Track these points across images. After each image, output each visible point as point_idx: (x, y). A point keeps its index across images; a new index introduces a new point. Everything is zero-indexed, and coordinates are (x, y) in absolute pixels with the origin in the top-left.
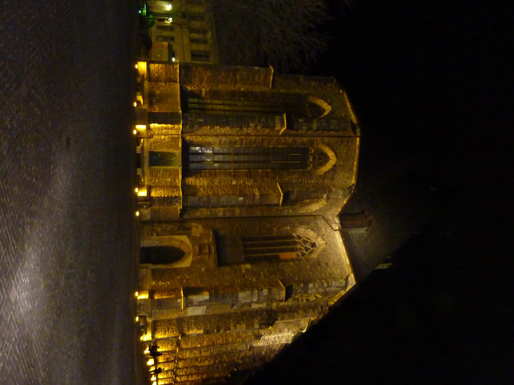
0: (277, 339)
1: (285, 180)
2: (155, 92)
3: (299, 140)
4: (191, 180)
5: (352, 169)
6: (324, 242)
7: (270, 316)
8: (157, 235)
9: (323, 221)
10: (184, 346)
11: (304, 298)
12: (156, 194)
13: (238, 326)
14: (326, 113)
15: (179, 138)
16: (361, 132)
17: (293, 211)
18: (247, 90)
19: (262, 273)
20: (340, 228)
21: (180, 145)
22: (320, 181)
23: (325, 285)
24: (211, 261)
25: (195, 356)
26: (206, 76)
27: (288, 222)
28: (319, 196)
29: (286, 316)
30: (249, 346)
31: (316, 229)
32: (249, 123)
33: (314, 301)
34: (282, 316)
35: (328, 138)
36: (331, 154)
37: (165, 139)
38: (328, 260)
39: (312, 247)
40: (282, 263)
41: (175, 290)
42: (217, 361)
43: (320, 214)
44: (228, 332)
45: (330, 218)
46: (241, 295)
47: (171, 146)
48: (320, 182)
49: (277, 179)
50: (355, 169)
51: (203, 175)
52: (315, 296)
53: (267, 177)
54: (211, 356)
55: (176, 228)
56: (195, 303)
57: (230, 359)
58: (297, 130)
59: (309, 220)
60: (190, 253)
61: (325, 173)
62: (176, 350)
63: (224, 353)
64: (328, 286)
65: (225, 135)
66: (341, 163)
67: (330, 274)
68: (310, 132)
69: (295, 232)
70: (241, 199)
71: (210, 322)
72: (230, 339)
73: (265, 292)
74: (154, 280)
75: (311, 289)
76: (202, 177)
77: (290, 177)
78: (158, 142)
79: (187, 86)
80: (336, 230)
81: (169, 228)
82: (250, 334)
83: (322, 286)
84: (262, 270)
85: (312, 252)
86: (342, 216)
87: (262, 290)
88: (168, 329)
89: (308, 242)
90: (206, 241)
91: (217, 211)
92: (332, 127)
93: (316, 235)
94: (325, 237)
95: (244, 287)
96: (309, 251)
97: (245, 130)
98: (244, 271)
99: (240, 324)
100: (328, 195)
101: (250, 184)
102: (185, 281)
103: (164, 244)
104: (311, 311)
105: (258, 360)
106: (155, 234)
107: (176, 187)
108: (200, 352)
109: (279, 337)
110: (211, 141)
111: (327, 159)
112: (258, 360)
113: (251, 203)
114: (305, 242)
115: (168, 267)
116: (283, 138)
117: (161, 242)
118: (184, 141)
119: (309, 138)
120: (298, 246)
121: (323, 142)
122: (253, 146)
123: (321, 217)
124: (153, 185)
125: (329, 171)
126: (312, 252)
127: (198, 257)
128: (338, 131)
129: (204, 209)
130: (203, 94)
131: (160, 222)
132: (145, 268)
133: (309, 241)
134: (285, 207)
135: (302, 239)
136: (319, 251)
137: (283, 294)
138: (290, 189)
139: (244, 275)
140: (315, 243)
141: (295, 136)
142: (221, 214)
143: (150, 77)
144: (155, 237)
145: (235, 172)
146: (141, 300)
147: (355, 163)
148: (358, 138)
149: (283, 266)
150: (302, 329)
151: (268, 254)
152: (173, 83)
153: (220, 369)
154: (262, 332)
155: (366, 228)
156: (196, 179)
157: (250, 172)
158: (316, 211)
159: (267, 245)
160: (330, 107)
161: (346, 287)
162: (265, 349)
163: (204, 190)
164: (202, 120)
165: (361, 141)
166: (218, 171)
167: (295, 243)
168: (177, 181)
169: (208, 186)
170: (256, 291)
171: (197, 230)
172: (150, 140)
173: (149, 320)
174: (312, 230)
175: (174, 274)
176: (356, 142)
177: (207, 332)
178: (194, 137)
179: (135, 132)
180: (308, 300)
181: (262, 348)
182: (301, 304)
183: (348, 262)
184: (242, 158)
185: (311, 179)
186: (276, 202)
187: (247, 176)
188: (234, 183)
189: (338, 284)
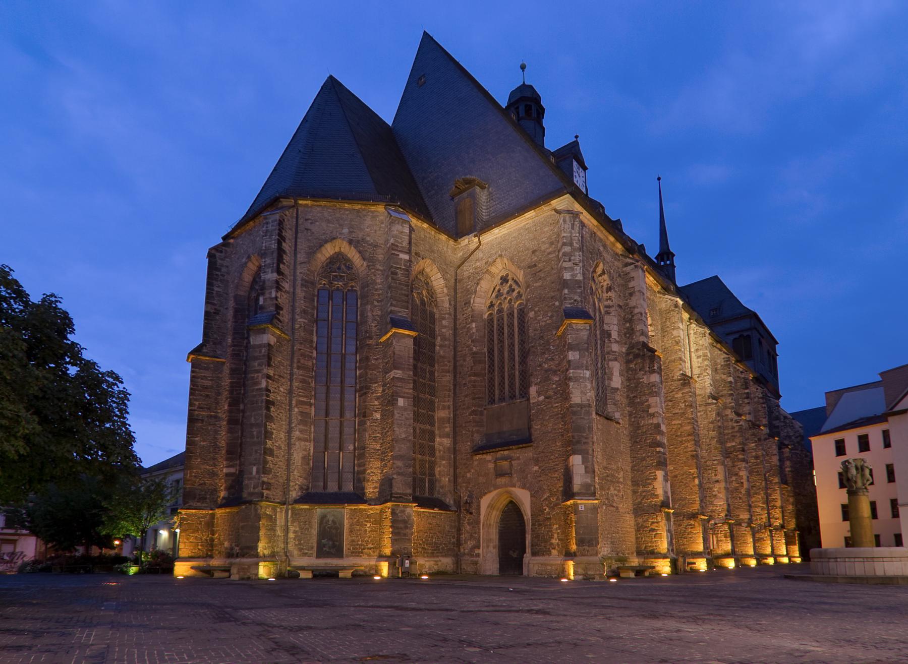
0: (700, 353)
1: (374, 329)
2: (226, 549)
3: (301, 304)
4: (371, 489)
5: (358, 211)
6: (499, 260)
7: (637, 356)
10: (696, 507)
11: (605, 295)
13: (651, 411)
17: (444, 319)
18: (227, 398)
21: (306, 507)
22: (378, 267)
25: (723, 490)
26: (203, 467)
29: (639, 327)
30: (710, 401)
32: (260, 389)
34: (638, 334)
35: (299, 256)
36: (329, 250)
37: (295, 532)
38: (528, 249)
39: (507, 282)
41: (566, 513)
42: (741, 457)
43: (453, 274)
44: (663, 428)
48: (381, 268)
49: (371, 342)
50: (357, 207)
51: (362, 468)
52: (600, 275)
53: (367, 358)
55: (468, 516)
56: (589, 480)
57: (738, 434)
59: (460, 291)
60: (507, 492)
61: (364, 259)
62: (703, 520)
64: (571, 245)
65: (289, 432)
66: (346, 231)
67: (552, 243)
68: (286, 286)
70: (401, 402)
71: (643, 459)
72: (688, 428)
73: (573, 356)
74: (550, 554)
76: (365, 470)
77: (370, 320)
78: (300, 544)
80: (480, 242)
81: (468, 528)
82: (680, 395)
83: (569, 256)
84: (540, 366)
85: (515, 282)
86: (456, 234)
87: (569, 361)
88: (653, 530)
89: (499, 291)
90: (491, 466)
91: (441, 448)
95: (565, 395)
96: (514, 286)
99: (649, 407)
101: (381, 389)
102: (554, 499)
104: (631, 284)
105: (747, 391)
107: (382, 512)
108: (717, 481)
109: (697, 350)
110: (301, 455)
111: (338, 262)
112: (747, 391)
113: (411, 386)
114: (499, 294)
115: (529, 527)
117: (490, 540)
118: (297, 501)
120: (505, 306)
122: (313, 384)
124: (377, 553)
125: (360, 252)
126: (515, 282)
129: (437, 470)
130: (232, 470)
131: (459, 543)
134: (437, 332)
136: (513, 268)
137: (578, 323)
139: (546, 398)
140: (501, 278)
141: (293, 312)
142: (447, 442)
143: (203, 557)
144: (480, 551)
145: (359, 415)
146: (575, 574)
147: (346, 205)
148: (300, 202)
149: (535, 330)
150: (676, 306)
151: (517, 359)
153: (760, 453)
156: (368, 481)
157: (361, 389)
159: (502, 361)
161: (576, 215)
163: (385, 465)
164: (255, 469)
165: (305, 198)
167: (500, 311)
169: (382, 460)
173: (635, 561)
174: (478, 284)
175: (541, 518)
176: (306, 205)
177: (662, 464)
178: (292, 484)
180: (609, 289)
183: (531, 214)
184: (335, 404)
185: (374, 282)
186: (411, 342)
187: (365, 393)
188: (378, 416)
189: (568, 226)
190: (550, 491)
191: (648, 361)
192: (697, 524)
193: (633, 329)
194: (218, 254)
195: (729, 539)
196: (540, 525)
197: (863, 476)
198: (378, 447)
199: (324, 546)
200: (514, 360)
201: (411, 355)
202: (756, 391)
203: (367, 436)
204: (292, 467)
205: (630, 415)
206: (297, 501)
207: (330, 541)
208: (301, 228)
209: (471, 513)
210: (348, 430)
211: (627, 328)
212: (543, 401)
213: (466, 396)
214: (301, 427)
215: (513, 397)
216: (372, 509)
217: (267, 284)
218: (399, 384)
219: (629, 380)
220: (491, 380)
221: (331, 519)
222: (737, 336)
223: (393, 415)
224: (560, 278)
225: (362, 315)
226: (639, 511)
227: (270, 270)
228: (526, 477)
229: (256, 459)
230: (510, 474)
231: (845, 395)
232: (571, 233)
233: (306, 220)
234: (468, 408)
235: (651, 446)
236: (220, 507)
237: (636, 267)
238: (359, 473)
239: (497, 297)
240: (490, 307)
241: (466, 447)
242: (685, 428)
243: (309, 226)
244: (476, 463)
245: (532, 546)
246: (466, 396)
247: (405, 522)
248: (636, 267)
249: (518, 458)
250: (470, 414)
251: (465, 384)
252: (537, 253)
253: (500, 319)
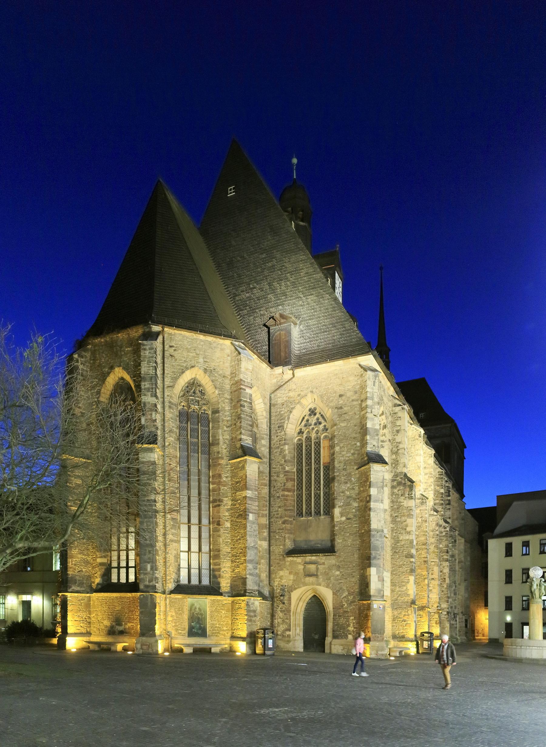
0: (427, 471)
4: (225, 584)
5: (210, 343)
6: (309, 395)
7: (399, 484)
8: (290, 630)
9: (279, 393)
12: (242, 630)
13: (408, 529)
14: (127, 377)
15: (170, 597)
16: (157, 323)
17: (263, 438)
19: (348, 493)
20: (290, 367)
27: (278, 448)
28: (248, 400)
31: (290, 405)
33: (387, 418)
34: (401, 465)
36: (187, 377)
37: (172, 616)
38: (335, 392)
39: (315, 414)
45: (275, 381)
53: (220, 476)
54: (439, 566)
55: (281, 605)
56: (380, 586)
57: (445, 539)
58: (157, 428)
63: (437, 547)
66: (201, 360)
67: (356, 392)
69: (292, 439)
70: (251, 517)
71: (400, 567)
72: (423, 538)
74: (346, 637)
75: (373, 425)
77: (221, 443)
79: (94, 582)
80: (294, 376)
81: (281, 615)
82: (418, 511)
84: (343, 492)
85: (322, 415)
89: (308, 421)
90: (301, 567)
92: (152, 372)
93: (298, 406)
94: (302, 393)
96: (321, 420)
97: (159, 506)
99: (407, 526)
101: (230, 503)
103: (302, 623)
104: (398, 423)
105: (449, 498)
106: (288, 633)
111: (193, 387)
112: (449, 498)
116: (167, 450)
118: (172, 592)
119: (167, 408)
121: (172, 387)
123: (272, 396)
124: (230, 633)
126: (322, 415)
128: (156, 362)
132: (331, 647)
133: (306, 418)
135: (304, 429)
136: (321, 405)
138: (238, 446)
139: (348, 519)
140: (310, 410)
142: (265, 544)
144: (291, 633)
145: (213, 522)
152: (92, 602)
154: (418, 495)
155: (292, 326)
156: (223, 577)
157: (214, 501)
158: (265, 404)
160: (117, 369)
161: (374, 370)
162: (438, 488)
164: (149, 567)
167: (309, 439)
168: (225, 602)
171: (284, 577)
172: (173, 635)
174: (291, 412)
177: (412, 571)
178: (168, 578)
179: (167, 654)
181: (436, 492)
182: (389, 436)
187: (219, 505)
188: (228, 525)
190: (348, 591)
192: (424, 615)
193: (398, 461)
195: (438, 625)
196: (340, 616)
197: (540, 590)
198: (229, 550)
200: (320, 483)
201: (257, 479)
202: (454, 496)
203: (221, 541)
204: (168, 564)
205: (392, 531)
206: (172, 592)
207: (197, 627)
208: (167, 354)
209: (284, 603)
210: (205, 535)
212: (345, 521)
213: (280, 507)
214: (173, 531)
215: (318, 513)
216: (226, 600)
219: (392, 502)
220: (300, 497)
221: (198, 607)
223: (245, 528)
225: (214, 436)
226: (395, 605)
227: (149, 393)
228: (329, 579)
229: (149, 558)
230: (316, 575)
231: (515, 503)
232: (373, 389)
233: (171, 347)
234: (281, 517)
235: (406, 557)
236: (97, 591)
237: (403, 408)
238: (214, 570)
239: (305, 426)
240: (299, 433)
241: (278, 549)
242: (421, 539)
244: (288, 563)
245: (333, 631)
246: (280, 507)
247: (254, 611)
248: (403, 408)
249: (324, 564)
250: (284, 523)
251: (278, 497)
252: (343, 398)
253: (309, 447)
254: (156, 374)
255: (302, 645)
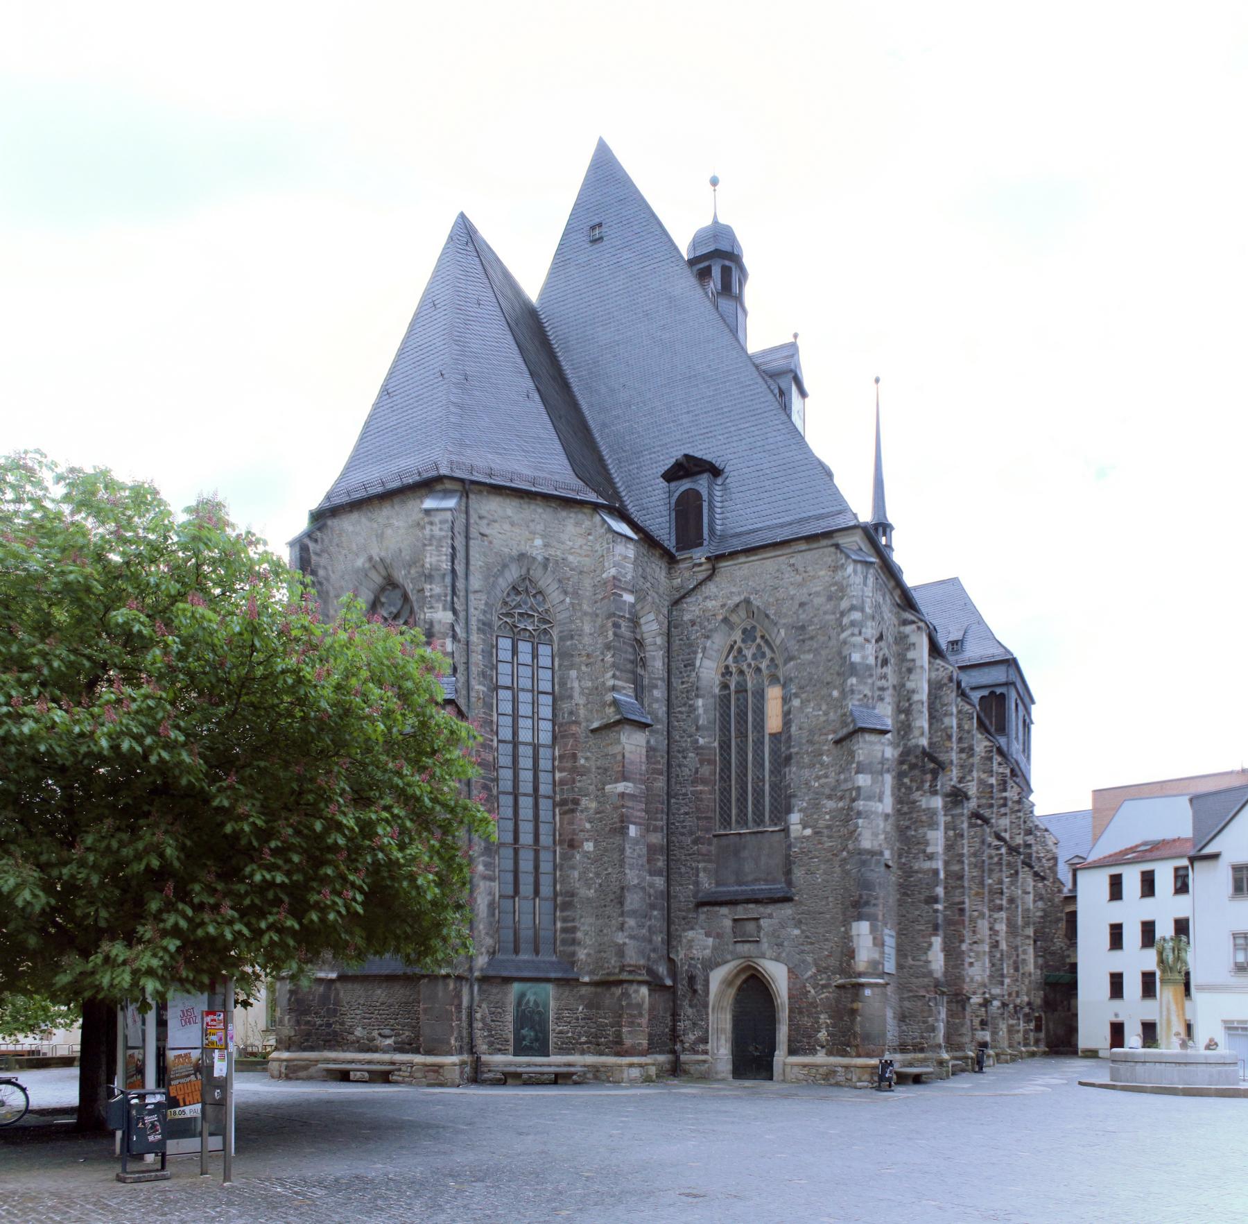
7: (913, 767)
13: (929, 850)
17: (656, 687)
22: (585, 607)
23: (856, 616)
24: (773, 918)
40: (793, 729)
46: (866, 844)
47: (500, 1005)
56: (876, 956)
61: (566, 593)
64: (862, 610)
67: (830, 598)
70: (633, 831)
73: (863, 780)
75: (864, 657)
87: (859, 788)
90: (996, 991)
98: (808, 832)
100: (624, 589)
103: (728, 1026)
104: (910, 655)
115: (783, 1015)
117: (723, 1031)
127: (765, 946)
131: (675, 1036)
139: (816, 833)
145: (561, 842)
157: (563, 802)
158: (660, 624)
159: (743, 765)
166: (558, 887)
170: (860, 805)
187: (573, 811)
190: (816, 965)
191: (929, 777)
193: (909, 726)
194: (311, 546)
199: (524, 1038)
208: (474, 532)
211: (902, 723)
217: (437, 628)
218: (630, 804)
220: (725, 792)
221: (532, 998)
222: (985, 693)
223: (622, 851)
224: (844, 659)
227: (441, 606)
231: (1128, 807)
237: (919, 628)
243: (485, 530)
248: (919, 628)
254: (453, 571)
255: (730, 1067)
